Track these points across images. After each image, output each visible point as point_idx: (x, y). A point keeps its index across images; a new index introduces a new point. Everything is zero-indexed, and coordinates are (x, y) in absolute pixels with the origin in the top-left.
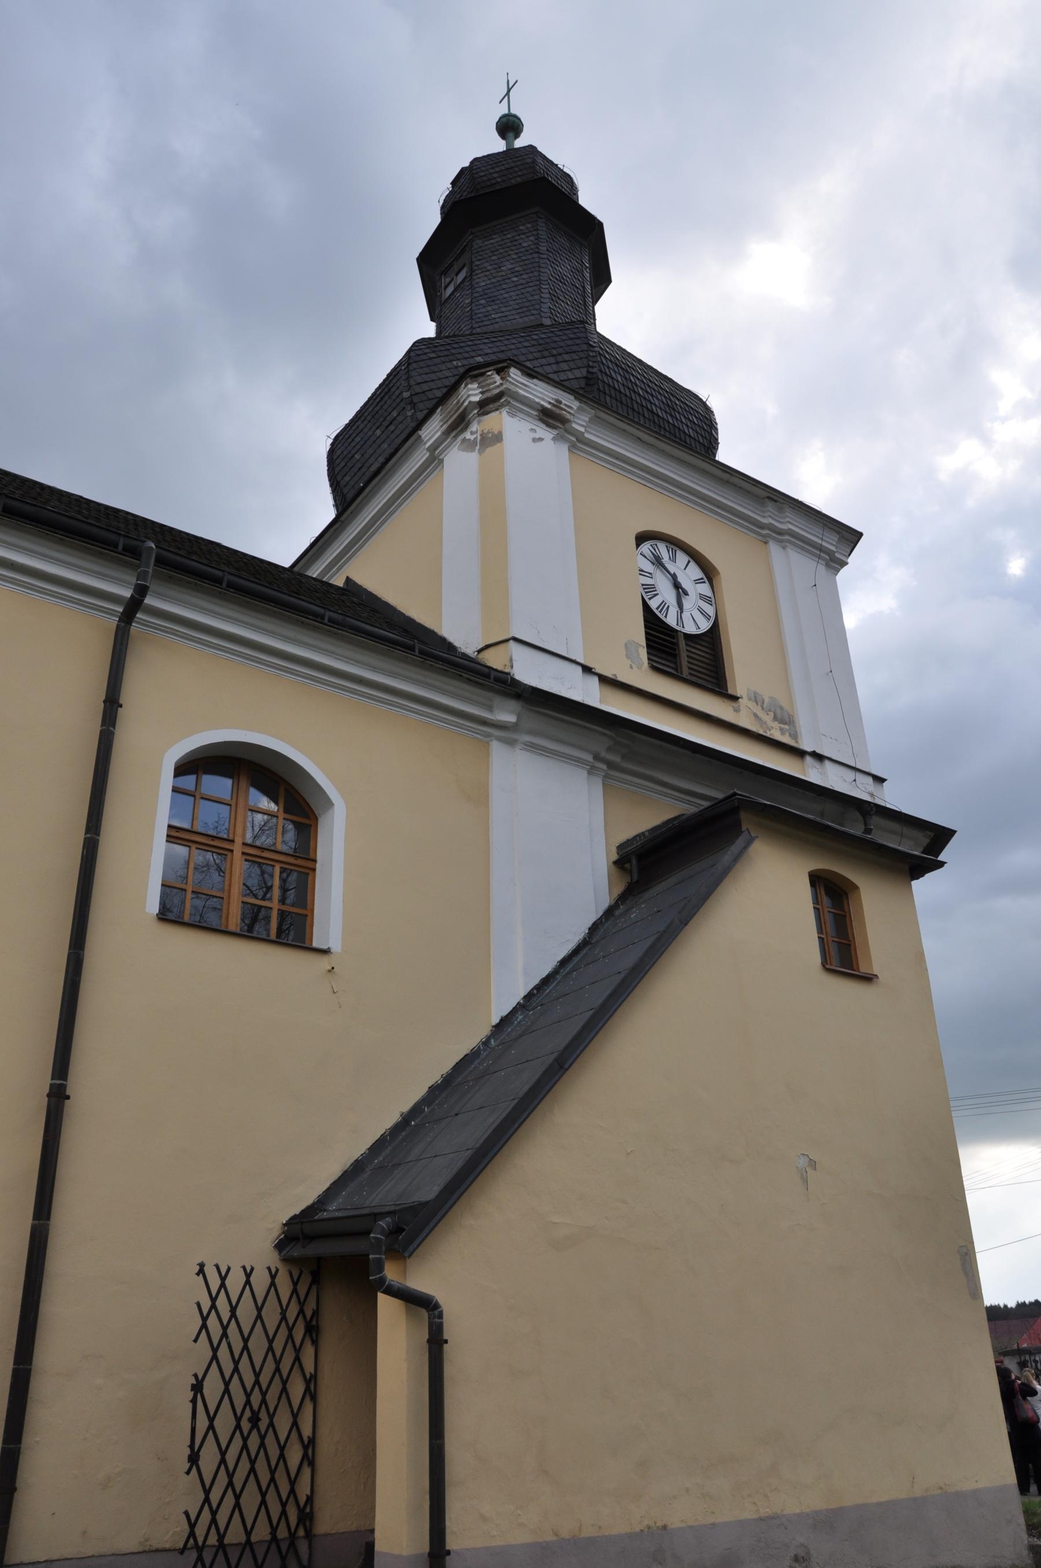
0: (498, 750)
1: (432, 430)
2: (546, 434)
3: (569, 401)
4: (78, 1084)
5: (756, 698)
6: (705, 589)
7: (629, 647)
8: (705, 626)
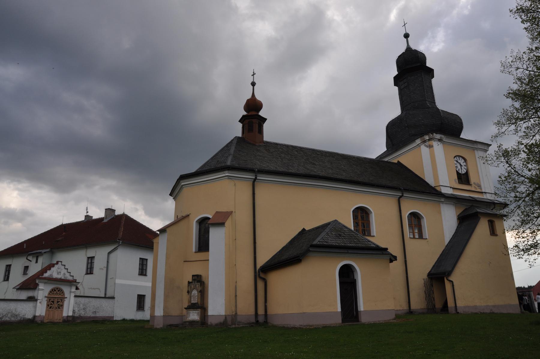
0: (441, 204)
1: (418, 141)
2: (439, 143)
3: (443, 136)
5: (474, 183)
6: (465, 164)
7: (455, 180)
8: (465, 171)
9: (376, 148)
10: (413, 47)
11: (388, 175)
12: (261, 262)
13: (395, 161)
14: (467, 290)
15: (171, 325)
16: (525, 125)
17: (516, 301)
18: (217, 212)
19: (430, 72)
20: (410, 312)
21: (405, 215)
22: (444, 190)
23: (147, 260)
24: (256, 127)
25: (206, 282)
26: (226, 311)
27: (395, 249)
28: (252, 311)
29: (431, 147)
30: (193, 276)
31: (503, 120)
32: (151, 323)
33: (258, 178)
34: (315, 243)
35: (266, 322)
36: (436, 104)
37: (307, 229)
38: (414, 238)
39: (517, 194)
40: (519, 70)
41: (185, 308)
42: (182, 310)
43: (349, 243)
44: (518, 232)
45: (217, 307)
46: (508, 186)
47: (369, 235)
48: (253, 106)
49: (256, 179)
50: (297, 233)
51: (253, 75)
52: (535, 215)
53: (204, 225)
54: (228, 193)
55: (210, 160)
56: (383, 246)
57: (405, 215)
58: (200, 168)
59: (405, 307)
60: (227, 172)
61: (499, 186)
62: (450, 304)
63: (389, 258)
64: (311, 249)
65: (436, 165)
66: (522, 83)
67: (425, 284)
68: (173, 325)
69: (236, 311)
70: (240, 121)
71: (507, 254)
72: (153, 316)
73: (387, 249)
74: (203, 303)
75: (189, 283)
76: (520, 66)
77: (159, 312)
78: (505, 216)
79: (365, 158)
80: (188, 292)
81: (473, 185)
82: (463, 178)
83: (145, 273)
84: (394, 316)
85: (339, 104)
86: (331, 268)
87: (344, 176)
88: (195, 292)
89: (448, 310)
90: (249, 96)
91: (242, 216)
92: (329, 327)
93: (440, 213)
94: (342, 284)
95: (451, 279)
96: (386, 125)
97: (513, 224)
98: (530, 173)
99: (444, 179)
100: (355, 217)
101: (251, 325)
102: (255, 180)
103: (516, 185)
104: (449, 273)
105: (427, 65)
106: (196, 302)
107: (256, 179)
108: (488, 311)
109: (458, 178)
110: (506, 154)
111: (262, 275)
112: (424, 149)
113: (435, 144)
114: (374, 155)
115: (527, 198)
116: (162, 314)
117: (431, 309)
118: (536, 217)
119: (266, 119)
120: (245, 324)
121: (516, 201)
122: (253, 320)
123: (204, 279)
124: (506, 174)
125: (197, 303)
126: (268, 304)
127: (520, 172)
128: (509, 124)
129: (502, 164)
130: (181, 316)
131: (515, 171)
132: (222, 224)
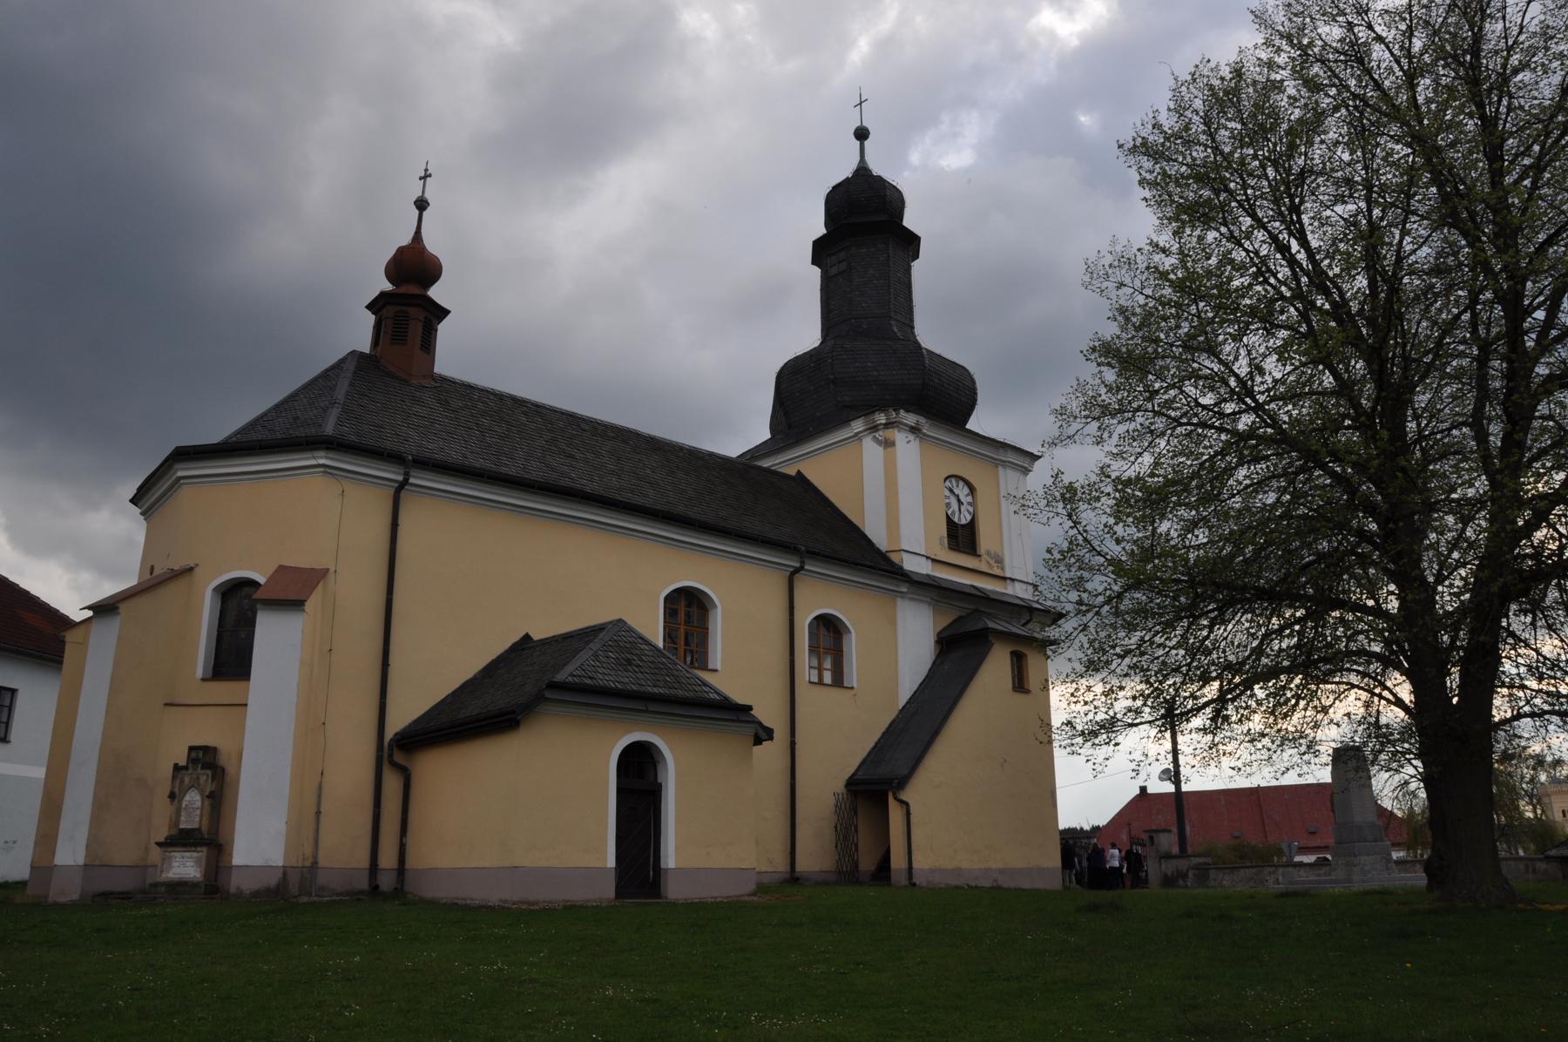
0: (899, 601)
1: (858, 425)
2: (911, 437)
3: (922, 420)
5: (988, 553)
6: (970, 499)
7: (941, 538)
8: (969, 518)
9: (741, 427)
10: (877, 169)
11: (764, 509)
12: (398, 720)
13: (791, 471)
14: (941, 830)
15: (106, 895)
16: (1122, 429)
17: (1056, 861)
19: (911, 243)
20: (794, 878)
21: (804, 621)
22: (912, 565)
23: (13, 691)
24: (416, 329)
25: (230, 770)
27: (769, 711)
28: (362, 859)
29: (889, 444)
30: (191, 749)
31: (1074, 406)
33: (412, 480)
34: (561, 677)
37: (536, 636)
38: (821, 682)
39: (1085, 596)
41: (158, 844)
43: (649, 684)
44: (1077, 690)
45: (260, 841)
46: (1066, 575)
47: (705, 667)
48: (414, 269)
49: (405, 482)
50: (506, 645)
51: (426, 177)
52: (1118, 650)
53: (240, 605)
54: (317, 514)
55: (269, 411)
56: (739, 698)
57: (804, 621)
59: (781, 865)
60: (322, 453)
61: (1045, 572)
62: (898, 861)
64: (548, 694)
65: (896, 494)
66: (1127, 319)
67: (838, 807)
68: (111, 893)
69: (315, 857)
70: (369, 307)
71: (1046, 740)
73: (750, 708)
75: (177, 768)
76: (1127, 281)
78: (1054, 642)
79: (712, 455)
80: (172, 796)
81: (985, 557)
82: (962, 537)
84: (752, 887)
85: (650, 286)
86: (603, 747)
87: (649, 499)
88: (193, 798)
89: (889, 878)
90: (406, 239)
91: (355, 587)
92: (581, 907)
93: (893, 622)
95: (904, 796)
96: (778, 369)
97: (1067, 668)
98: (1119, 548)
99: (913, 537)
101: (355, 896)
102: (402, 485)
103: (1086, 575)
104: (902, 782)
106: (196, 826)
107: (405, 482)
108: (987, 884)
109: (949, 535)
110: (1070, 496)
111: (399, 758)
112: (871, 450)
113: (900, 438)
114: (733, 446)
115: (1107, 608)
116: (81, 860)
117: (847, 874)
118: (1119, 656)
120: (338, 894)
121: (1079, 612)
122: (363, 884)
123: (223, 760)
124: (1065, 545)
125: (199, 830)
127: (1096, 543)
128: (1086, 417)
129: (1058, 520)
130: (143, 868)
131: (1085, 539)
132: (296, 604)
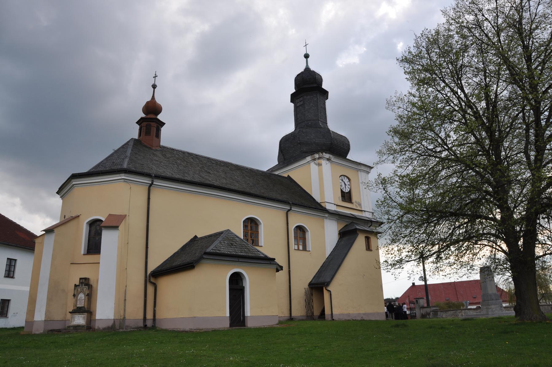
0: (325, 220)
1: (309, 159)
2: (328, 162)
3: (331, 156)
4: (291, 270)
5: (356, 202)
6: (349, 183)
7: (339, 197)
8: (349, 190)
9: (267, 159)
10: (312, 68)
11: (276, 189)
12: (152, 267)
14: (344, 300)
18: (110, 215)
19: (325, 94)
20: (291, 319)
22: (329, 207)
23: (15, 260)
24: (154, 130)
25: (94, 286)
26: (115, 316)
27: (281, 260)
28: (141, 316)
29: (319, 165)
30: (80, 279)
31: (384, 150)
32: (25, 330)
35: (154, 327)
36: (328, 125)
37: (199, 237)
38: (298, 249)
39: (390, 217)
40: (400, 109)
42: (66, 314)
43: (240, 252)
45: (105, 311)
46: (383, 210)
48: (152, 109)
51: (155, 77)
53: (96, 228)
54: (121, 196)
58: (94, 168)
59: (286, 314)
60: (123, 175)
61: (376, 209)
62: (327, 312)
63: (275, 267)
69: (124, 315)
70: (137, 123)
72: (30, 322)
73: (274, 259)
74: (90, 308)
75: (76, 286)
76: (401, 106)
77: (40, 316)
79: (258, 170)
80: (74, 295)
81: (355, 203)
82: (347, 196)
83: (12, 275)
84: (277, 322)
87: (236, 187)
88: (82, 296)
89: (325, 318)
90: (149, 99)
91: (135, 222)
94: (232, 290)
95: (329, 288)
96: (280, 139)
98: (402, 200)
99: (329, 198)
100: (245, 226)
101: (139, 329)
102: (151, 185)
103: (390, 209)
104: (328, 284)
105: (323, 87)
108: (359, 319)
110: (384, 182)
111: (152, 280)
114: (265, 168)
115: (398, 221)
116: (43, 319)
117: (310, 317)
119: (164, 124)
121: (388, 222)
122: (141, 324)
123: (91, 283)
124: (383, 199)
125: (84, 307)
126: (157, 309)
127: (393, 198)
128: (389, 154)
129: (380, 190)
130: (65, 321)
132: (116, 227)
